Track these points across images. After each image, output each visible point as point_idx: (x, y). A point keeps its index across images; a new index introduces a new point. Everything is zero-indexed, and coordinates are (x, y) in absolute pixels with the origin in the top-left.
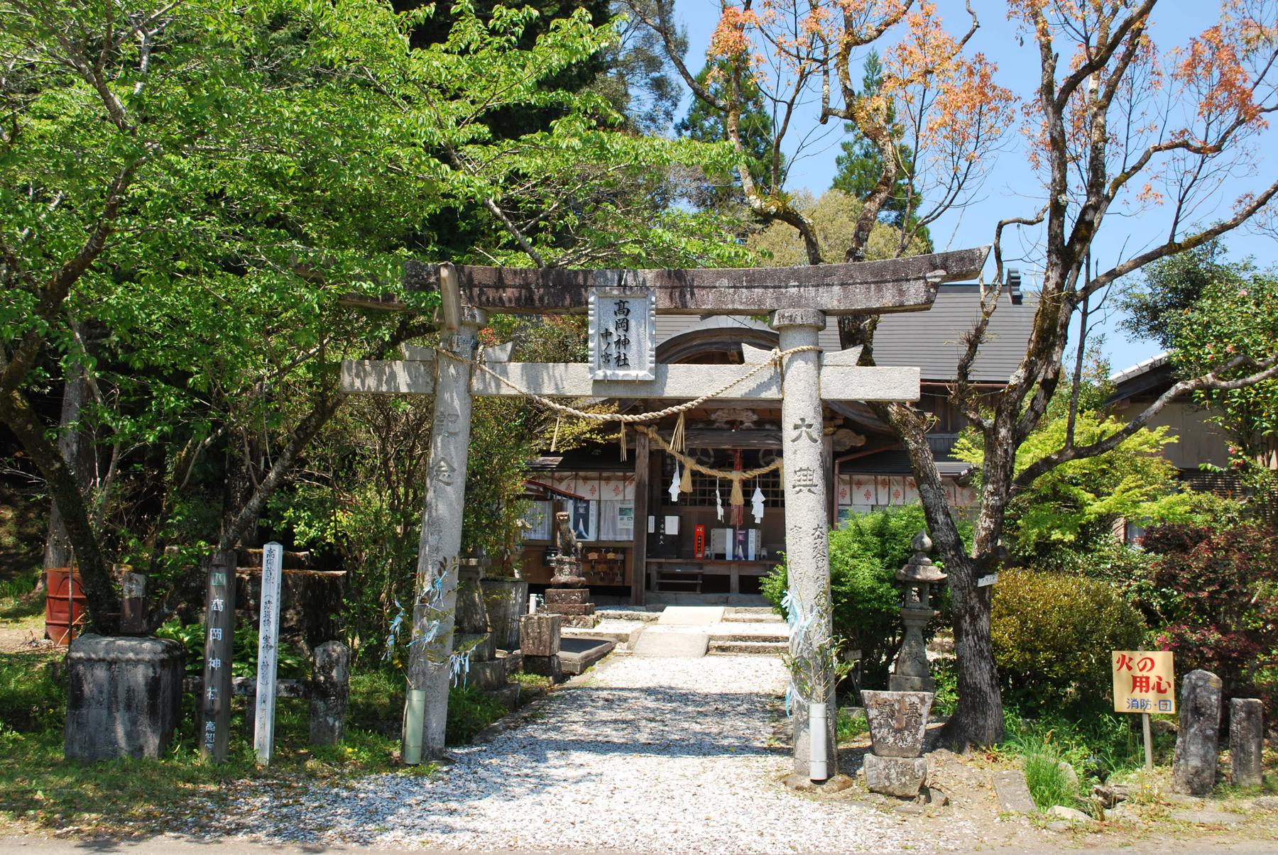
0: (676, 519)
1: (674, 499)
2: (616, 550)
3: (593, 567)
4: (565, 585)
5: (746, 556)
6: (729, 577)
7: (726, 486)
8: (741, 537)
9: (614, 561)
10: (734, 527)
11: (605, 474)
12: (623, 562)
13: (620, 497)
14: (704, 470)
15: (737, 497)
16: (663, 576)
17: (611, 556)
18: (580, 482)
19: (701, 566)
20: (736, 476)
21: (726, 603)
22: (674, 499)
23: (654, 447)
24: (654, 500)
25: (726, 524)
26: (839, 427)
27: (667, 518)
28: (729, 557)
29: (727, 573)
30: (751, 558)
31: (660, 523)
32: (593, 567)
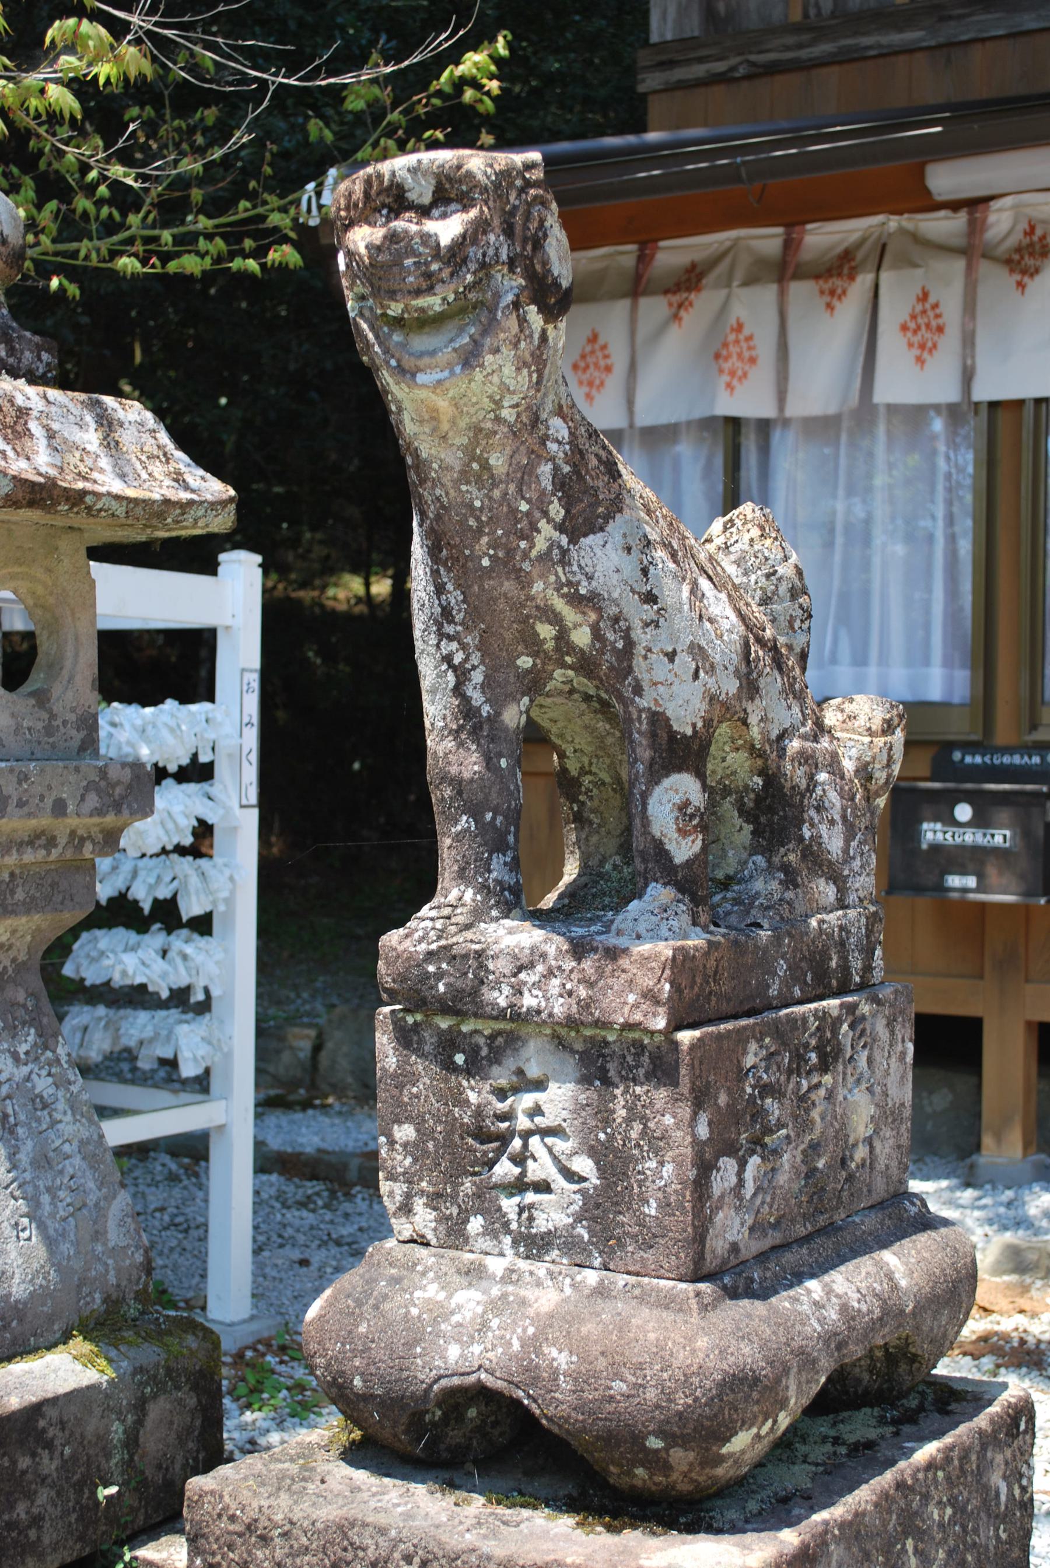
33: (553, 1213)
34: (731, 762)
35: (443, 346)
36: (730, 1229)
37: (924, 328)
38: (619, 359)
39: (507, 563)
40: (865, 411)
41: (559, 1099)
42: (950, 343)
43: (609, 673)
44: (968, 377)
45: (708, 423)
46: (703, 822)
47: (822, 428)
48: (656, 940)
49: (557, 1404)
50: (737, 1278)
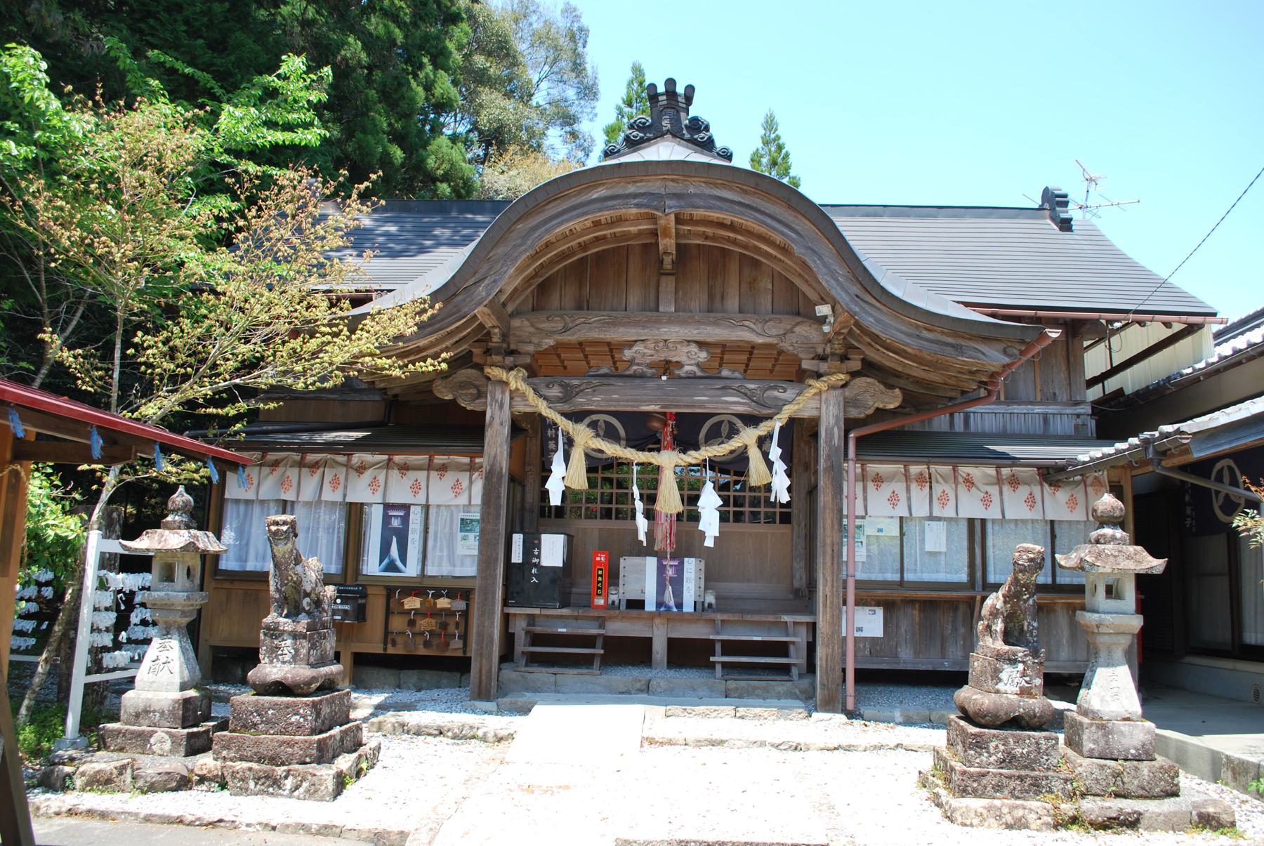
0: (560, 539)
1: (555, 500)
2: (452, 593)
3: (412, 623)
4: (280, 688)
5: (679, 605)
6: (649, 641)
7: (651, 476)
8: (395, 523)
9: (449, 613)
10: (660, 556)
11: (439, 459)
12: (466, 614)
13: (463, 500)
14: (612, 450)
15: (670, 500)
16: (536, 639)
17: (443, 603)
18: (395, 473)
19: (601, 621)
20: (669, 460)
21: (645, 692)
22: (555, 500)
23: (521, 408)
24: (523, 508)
25: (648, 551)
26: (854, 375)
27: (544, 537)
28: (650, 606)
29: (645, 634)
30: (688, 607)
31: (531, 546)
32: (412, 623)
33: (287, 658)
34: (313, 595)
35: (283, 542)
36: (312, 659)
37: (335, 483)
38: (255, 482)
39: (286, 569)
40: (319, 502)
41: (289, 642)
42: (341, 487)
43: (298, 584)
44: (345, 496)
45: (278, 501)
46: (309, 604)
47: (308, 504)
48: (304, 621)
49: (289, 681)
50: (313, 666)
